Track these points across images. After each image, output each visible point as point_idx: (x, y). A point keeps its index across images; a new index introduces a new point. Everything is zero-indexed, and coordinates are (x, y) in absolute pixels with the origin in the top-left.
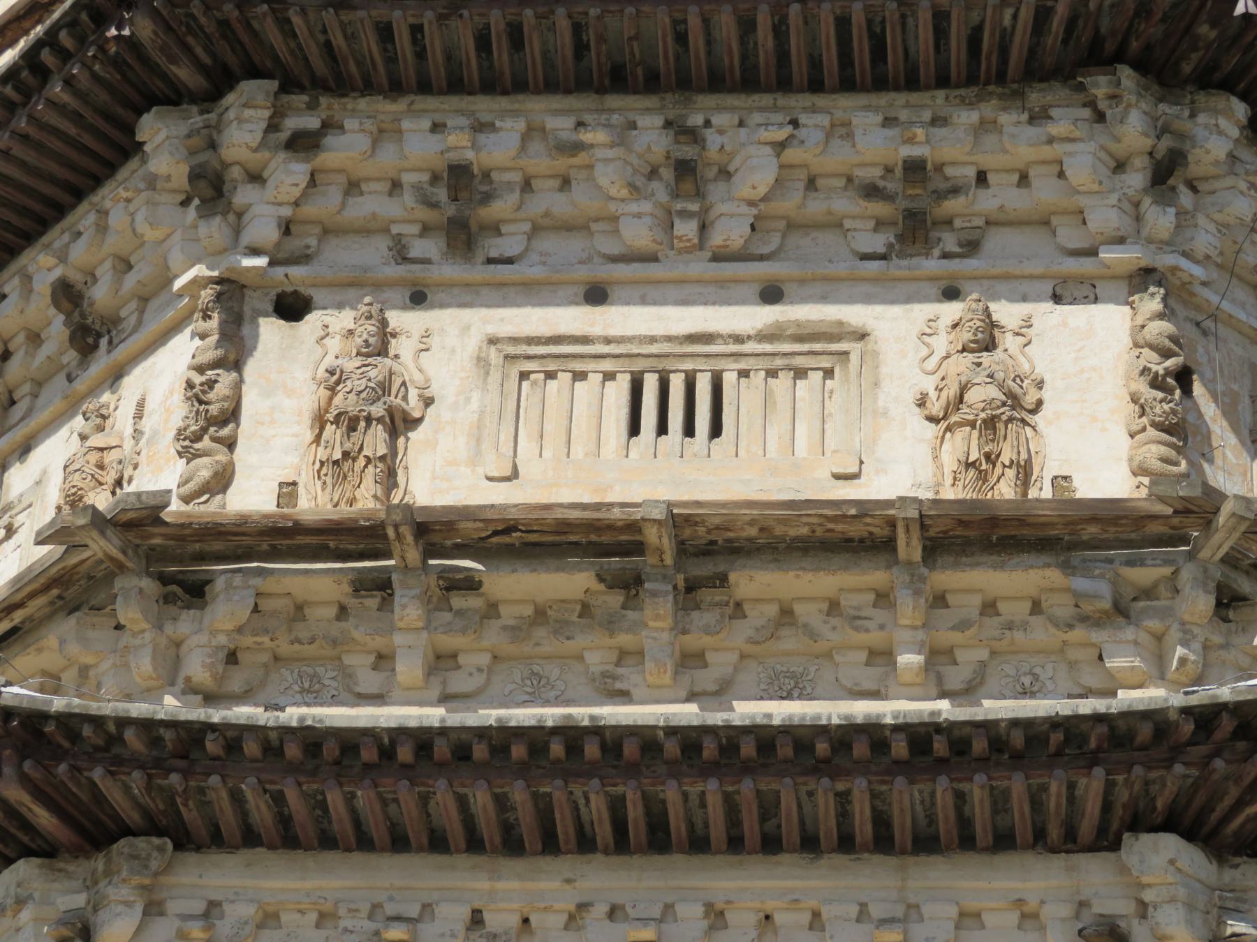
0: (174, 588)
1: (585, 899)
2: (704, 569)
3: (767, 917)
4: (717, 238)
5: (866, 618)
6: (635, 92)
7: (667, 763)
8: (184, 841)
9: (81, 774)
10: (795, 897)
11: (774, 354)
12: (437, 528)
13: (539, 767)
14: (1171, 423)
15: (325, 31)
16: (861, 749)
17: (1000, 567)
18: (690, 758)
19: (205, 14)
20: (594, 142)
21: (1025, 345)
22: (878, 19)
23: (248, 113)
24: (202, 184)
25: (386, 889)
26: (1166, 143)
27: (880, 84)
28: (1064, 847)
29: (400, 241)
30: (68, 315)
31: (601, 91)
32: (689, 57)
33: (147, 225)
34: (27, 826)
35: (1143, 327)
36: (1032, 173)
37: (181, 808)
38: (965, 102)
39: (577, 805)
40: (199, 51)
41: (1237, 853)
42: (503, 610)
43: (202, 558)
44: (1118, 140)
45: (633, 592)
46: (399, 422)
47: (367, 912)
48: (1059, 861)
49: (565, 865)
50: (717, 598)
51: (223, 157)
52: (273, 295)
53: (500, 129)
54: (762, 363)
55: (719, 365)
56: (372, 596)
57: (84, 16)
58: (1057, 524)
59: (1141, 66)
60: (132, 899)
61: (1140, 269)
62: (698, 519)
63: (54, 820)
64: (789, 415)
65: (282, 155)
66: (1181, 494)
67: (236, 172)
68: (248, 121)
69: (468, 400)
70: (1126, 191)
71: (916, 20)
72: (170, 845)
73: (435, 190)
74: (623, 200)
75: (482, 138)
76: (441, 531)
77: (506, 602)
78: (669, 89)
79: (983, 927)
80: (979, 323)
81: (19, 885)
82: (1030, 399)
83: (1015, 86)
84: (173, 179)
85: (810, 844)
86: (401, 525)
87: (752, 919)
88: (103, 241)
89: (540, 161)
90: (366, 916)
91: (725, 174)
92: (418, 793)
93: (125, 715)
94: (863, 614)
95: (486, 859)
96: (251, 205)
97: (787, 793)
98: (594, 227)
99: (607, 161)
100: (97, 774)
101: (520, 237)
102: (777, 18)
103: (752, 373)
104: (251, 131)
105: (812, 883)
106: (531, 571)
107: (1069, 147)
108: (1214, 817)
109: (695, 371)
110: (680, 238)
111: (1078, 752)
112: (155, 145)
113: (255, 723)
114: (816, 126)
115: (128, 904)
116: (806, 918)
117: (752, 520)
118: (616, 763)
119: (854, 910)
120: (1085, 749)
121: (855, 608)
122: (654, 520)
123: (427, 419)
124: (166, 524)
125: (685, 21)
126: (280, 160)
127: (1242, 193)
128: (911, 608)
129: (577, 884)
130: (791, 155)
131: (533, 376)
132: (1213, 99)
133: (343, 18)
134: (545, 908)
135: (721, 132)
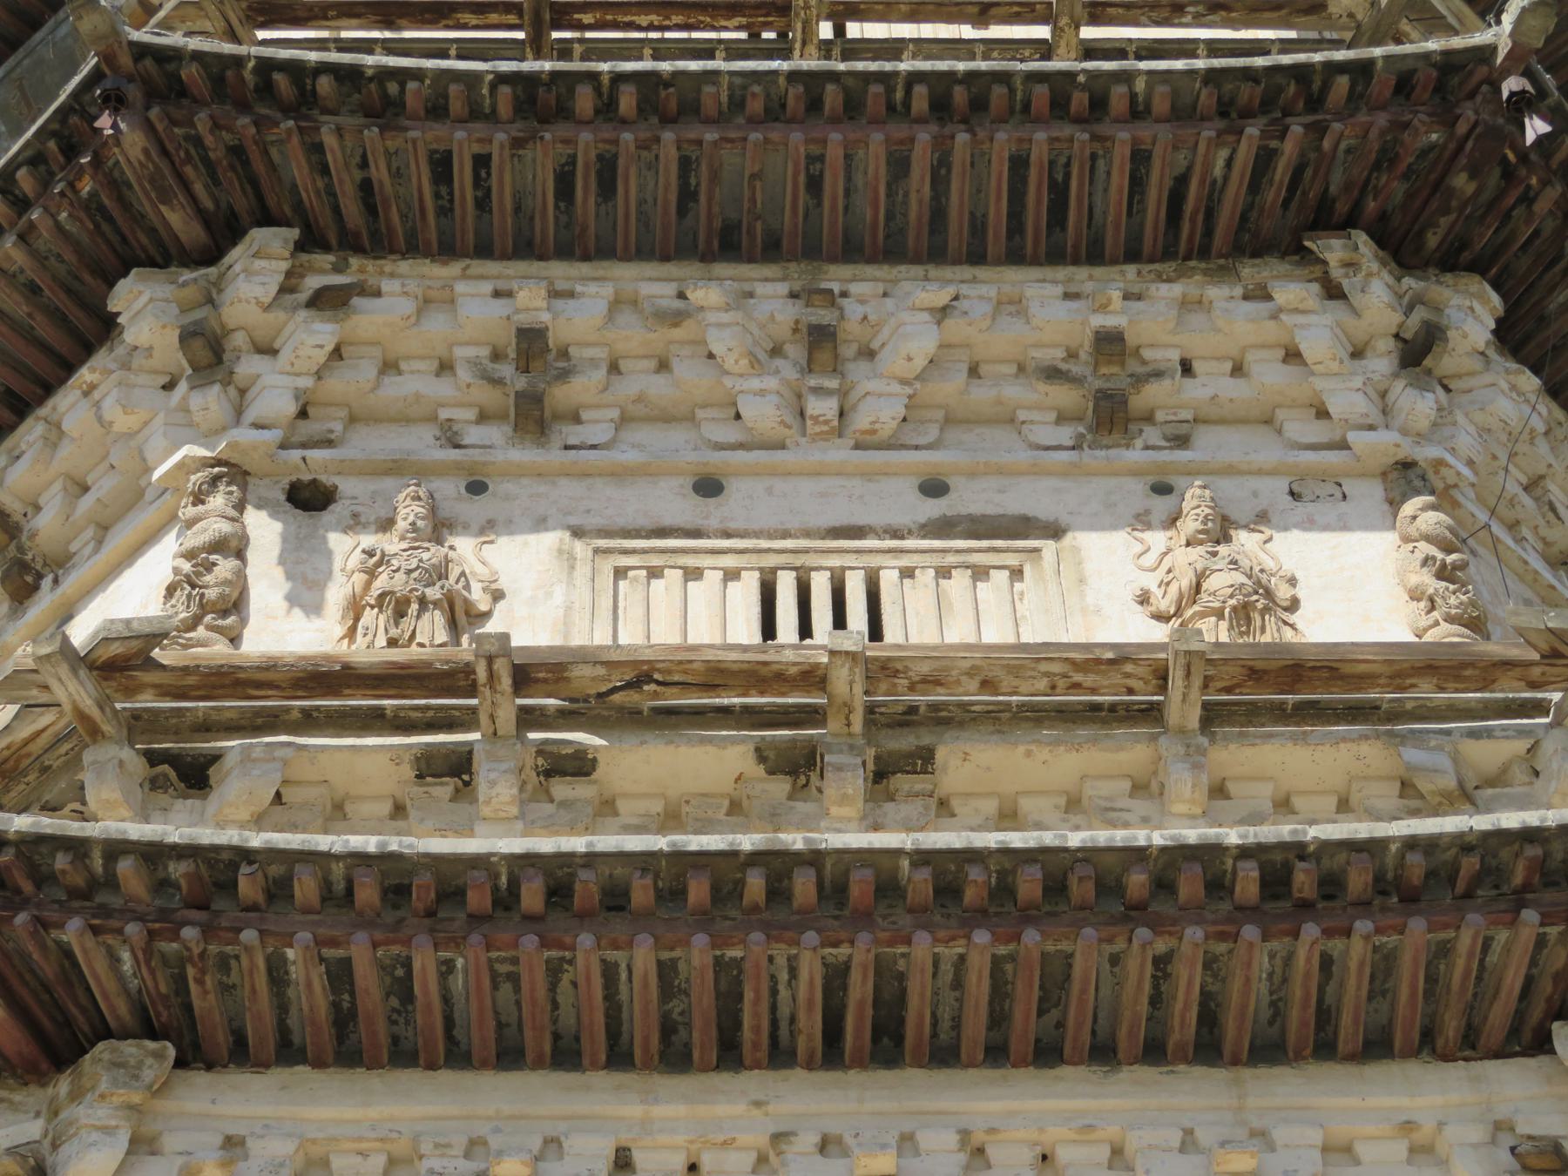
0: (165, 768)
1: (782, 1128)
2: (903, 742)
3: (1044, 1157)
4: (861, 421)
5: (1121, 810)
6: (751, 260)
7: (910, 911)
9: (48, 934)
10: (1087, 1122)
11: (944, 551)
12: (541, 675)
13: (726, 918)
14: (1471, 617)
15: (364, 164)
16: (1190, 885)
17: (1303, 739)
18: (943, 906)
19: (211, 131)
20: (705, 304)
21: (1265, 542)
22: (1063, 160)
23: (259, 264)
24: (198, 344)
25: (489, 1118)
26: (1420, 314)
27: (1056, 256)
28: (1459, 1054)
29: (450, 428)
31: (707, 257)
32: (821, 214)
33: (119, 409)
35: (1414, 518)
36: (1250, 357)
37: (193, 986)
38: (1160, 278)
39: (776, 983)
40: (198, 188)
42: (621, 805)
43: (207, 728)
44: (1356, 313)
45: (802, 780)
46: (462, 619)
47: (463, 1148)
48: (1457, 1070)
49: (753, 1082)
50: (918, 787)
51: (225, 318)
52: (285, 483)
53: (582, 295)
54: (929, 559)
55: (875, 561)
56: (442, 784)
57: (52, 145)
58: (1379, 676)
59: (1380, 240)
60: (113, 1123)
61: (1396, 463)
62: (899, 666)
64: (971, 614)
65: (303, 314)
66: (1550, 625)
67: (239, 339)
68: (257, 273)
69: (549, 595)
70: (1371, 376)
71: (1110, 164)
73: (497, 366)
74: (741, 376)
75: (559, 304)
76: (545, 681)
77: (625, 795)
78: (793, 258)
79: (1357, 1162)
80: (1208, 511)
83: (1222, 261)
84: (156, 353)
85: (1103, 1053)
86: (497, 657)
88: (52, 458)
89: (632, 335)
90: (462, 1154)
91: (869, 354)
92: (548, 961)
93: (120, 837)
94: (1119, 805)
95: (635, 1076)
96: (259, 376)
98: (700, 414)
99: (720, 325)
100: (72, 932)
101: (605, 426)
102: (936, 155)
103: (917, 572)
104: (264, 284)
105: (1110, 1103)
106: (666, 744)
107: (1300, 319)
109: (843, 569)
110: (815, 419)
111: (1494, 892)
112: (132, 313)
113: (313, 848)
114: (981, 297)
115: (107, 1130)
116: (1104, 1152)
117: (973, 667)
118: (837, 913)
119: (1176, 1138)
120: (1505, 889)
121: (1106, 799)
122: (847, 653)
123: (496, 613)
124: (163, 667)
125: (821, 158)
126: (301, 319)
127: (1502, 391)
128: (1190, 785)
129: (770, 1108)
130: (956, 327)
131: (631, 574)
132: (1464, 281)
133: (389, 143)
134: (725, 1143)
135: (862, 302)
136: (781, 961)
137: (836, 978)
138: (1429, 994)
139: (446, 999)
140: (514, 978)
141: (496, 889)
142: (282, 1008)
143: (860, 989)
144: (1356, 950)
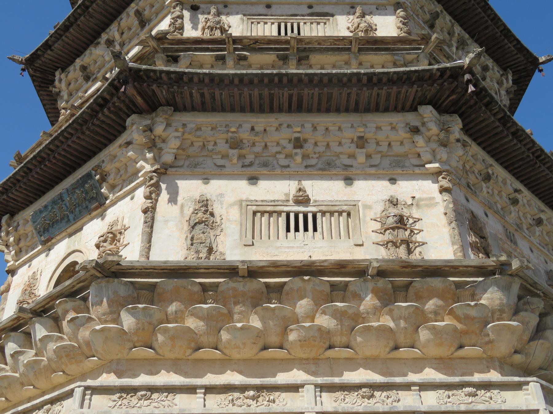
2: (304, 54)
8: (177, 109)
16: (354, 80)
30: (138, 18)
34: (134, 104)
37: (176, 97)
41: (444, 113)
48: (400, 114)
49: (276, 115)
50: (306, 63)
52: (190, 5)
55: (299, 21)
63: (142, 101)
69: (239, 27)
72: (173, 109)
79: (382, 130)
81: (132, 120)
82: (374, 27)
87: (324, 128)
97: (335, 91)
100: (154, 87)
105: (338, 119)
108: (441, 101)
109: (293, 22)
115: (162, 122)
116: (337, 128)
119: (350, 125)
129: (279, 120)
136: (281, 93)
137: (291, 96)
138: (396, 100)
139: (221, 100)
140: (233, 96)
141: (230, 80)
142: (192, 101)
143: (295, 99)
144: (383, 92)
